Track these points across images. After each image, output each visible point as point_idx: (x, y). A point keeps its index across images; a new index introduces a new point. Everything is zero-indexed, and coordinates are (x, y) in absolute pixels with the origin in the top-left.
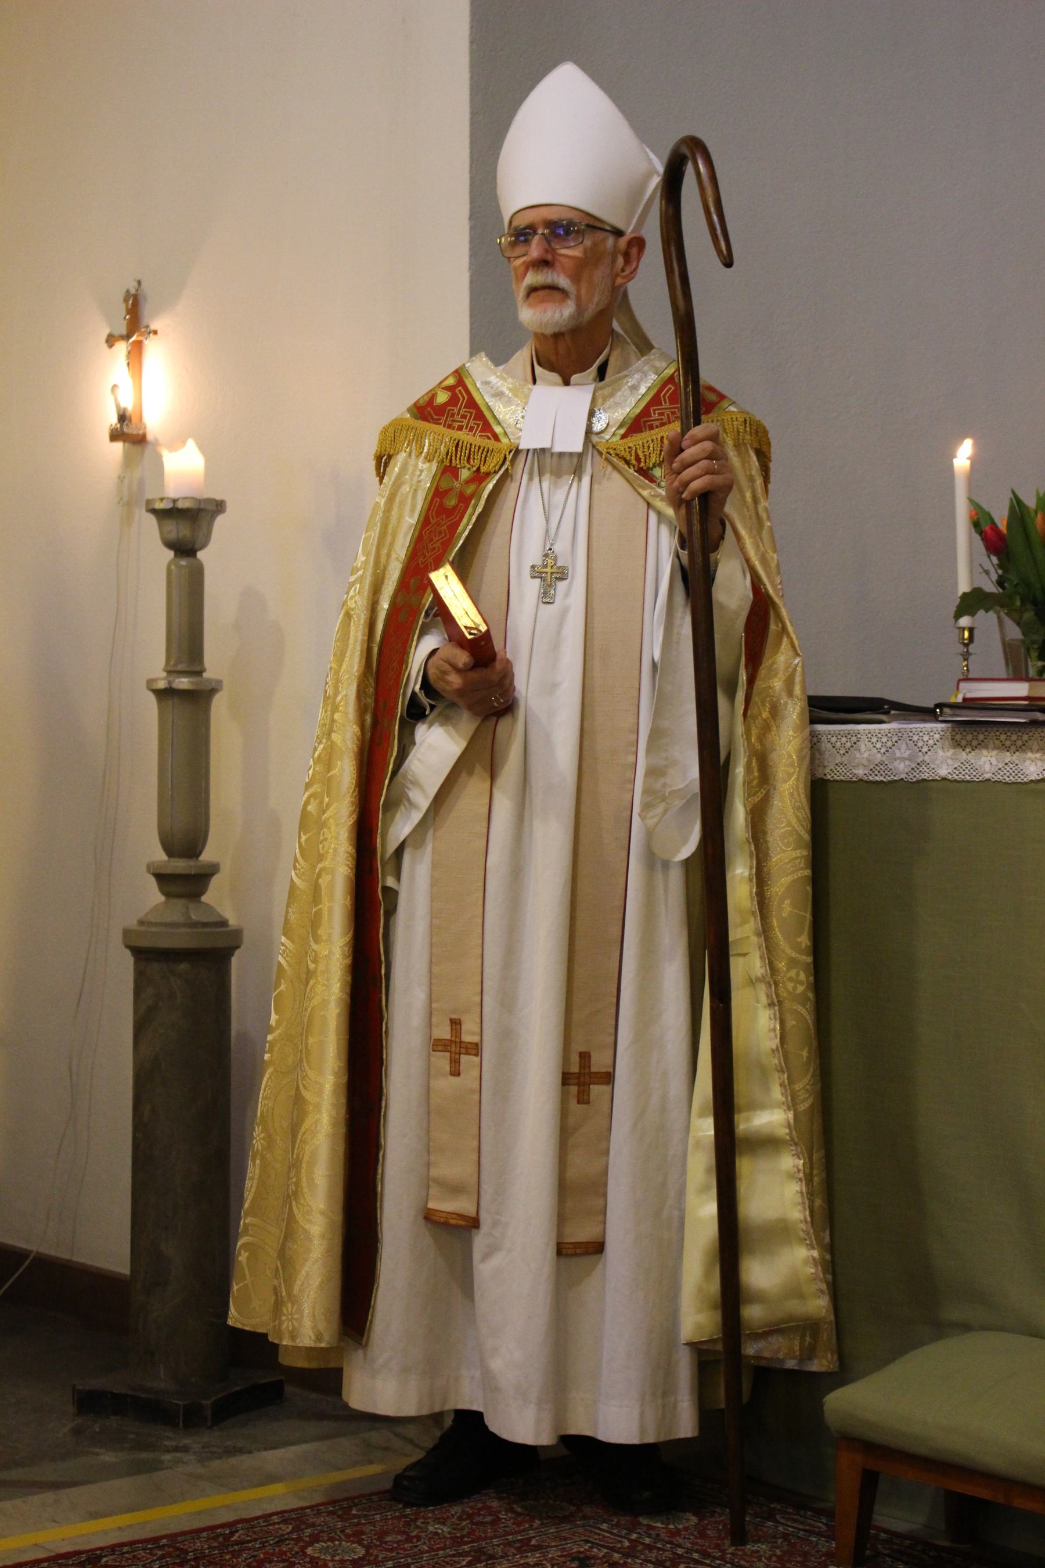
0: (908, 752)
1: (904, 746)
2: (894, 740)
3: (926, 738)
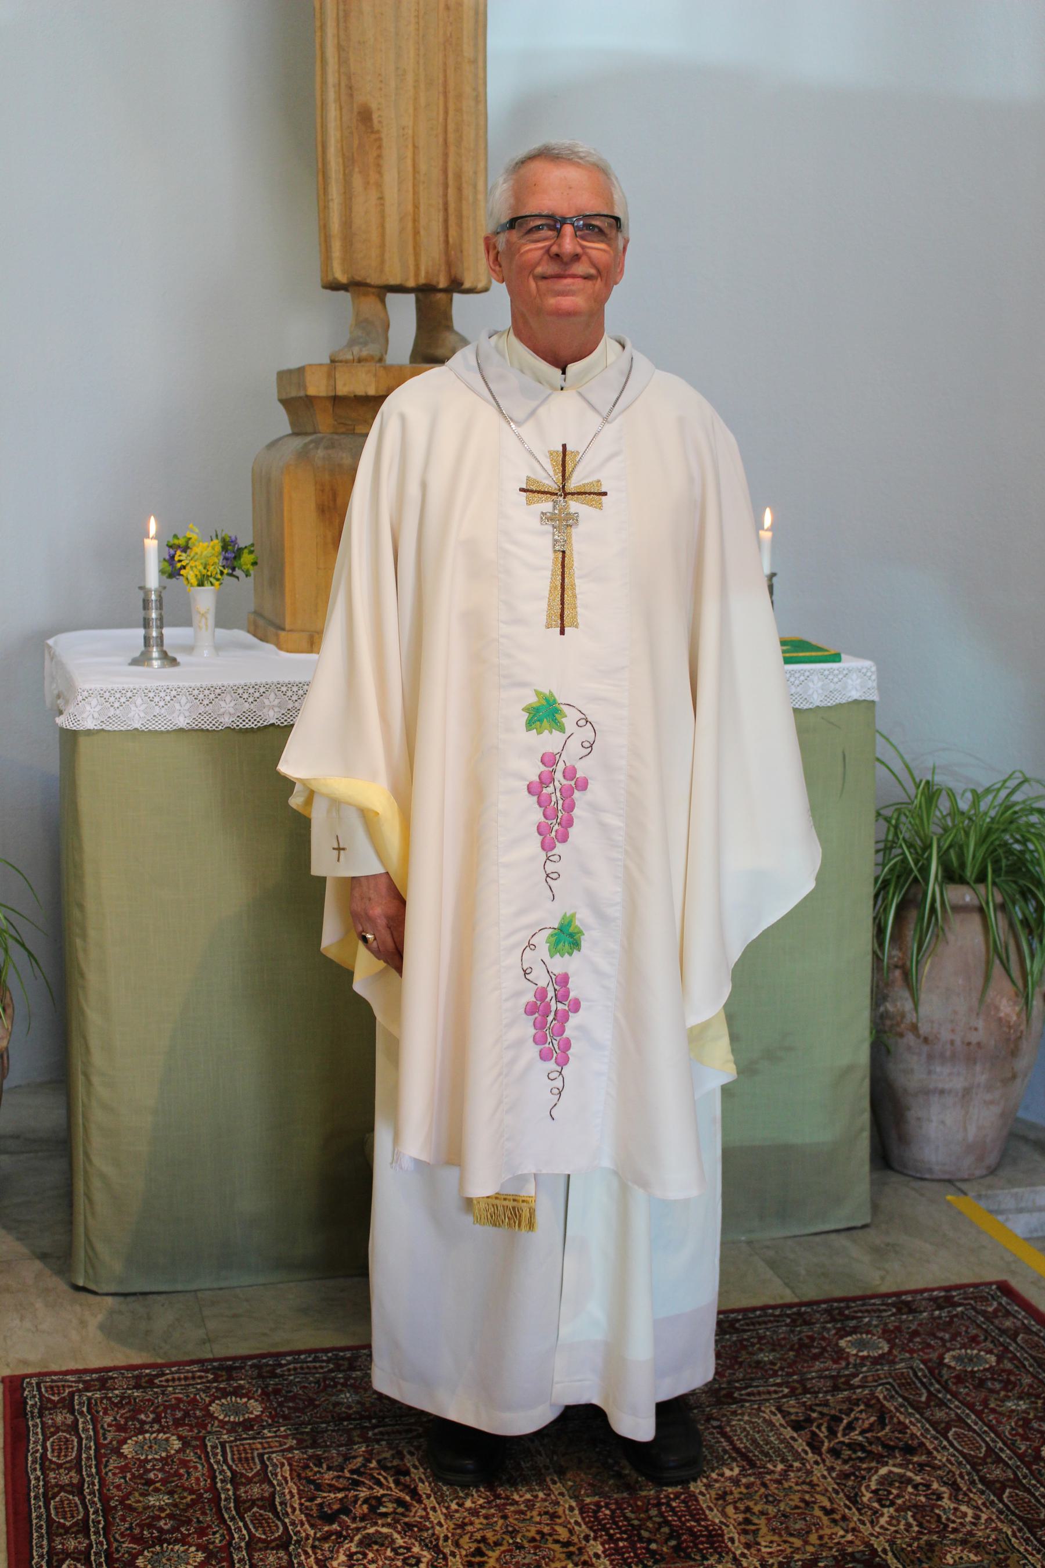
0: (277, 702)
1: (272, 696)
2: (261, 691)
3: (162, 694)
